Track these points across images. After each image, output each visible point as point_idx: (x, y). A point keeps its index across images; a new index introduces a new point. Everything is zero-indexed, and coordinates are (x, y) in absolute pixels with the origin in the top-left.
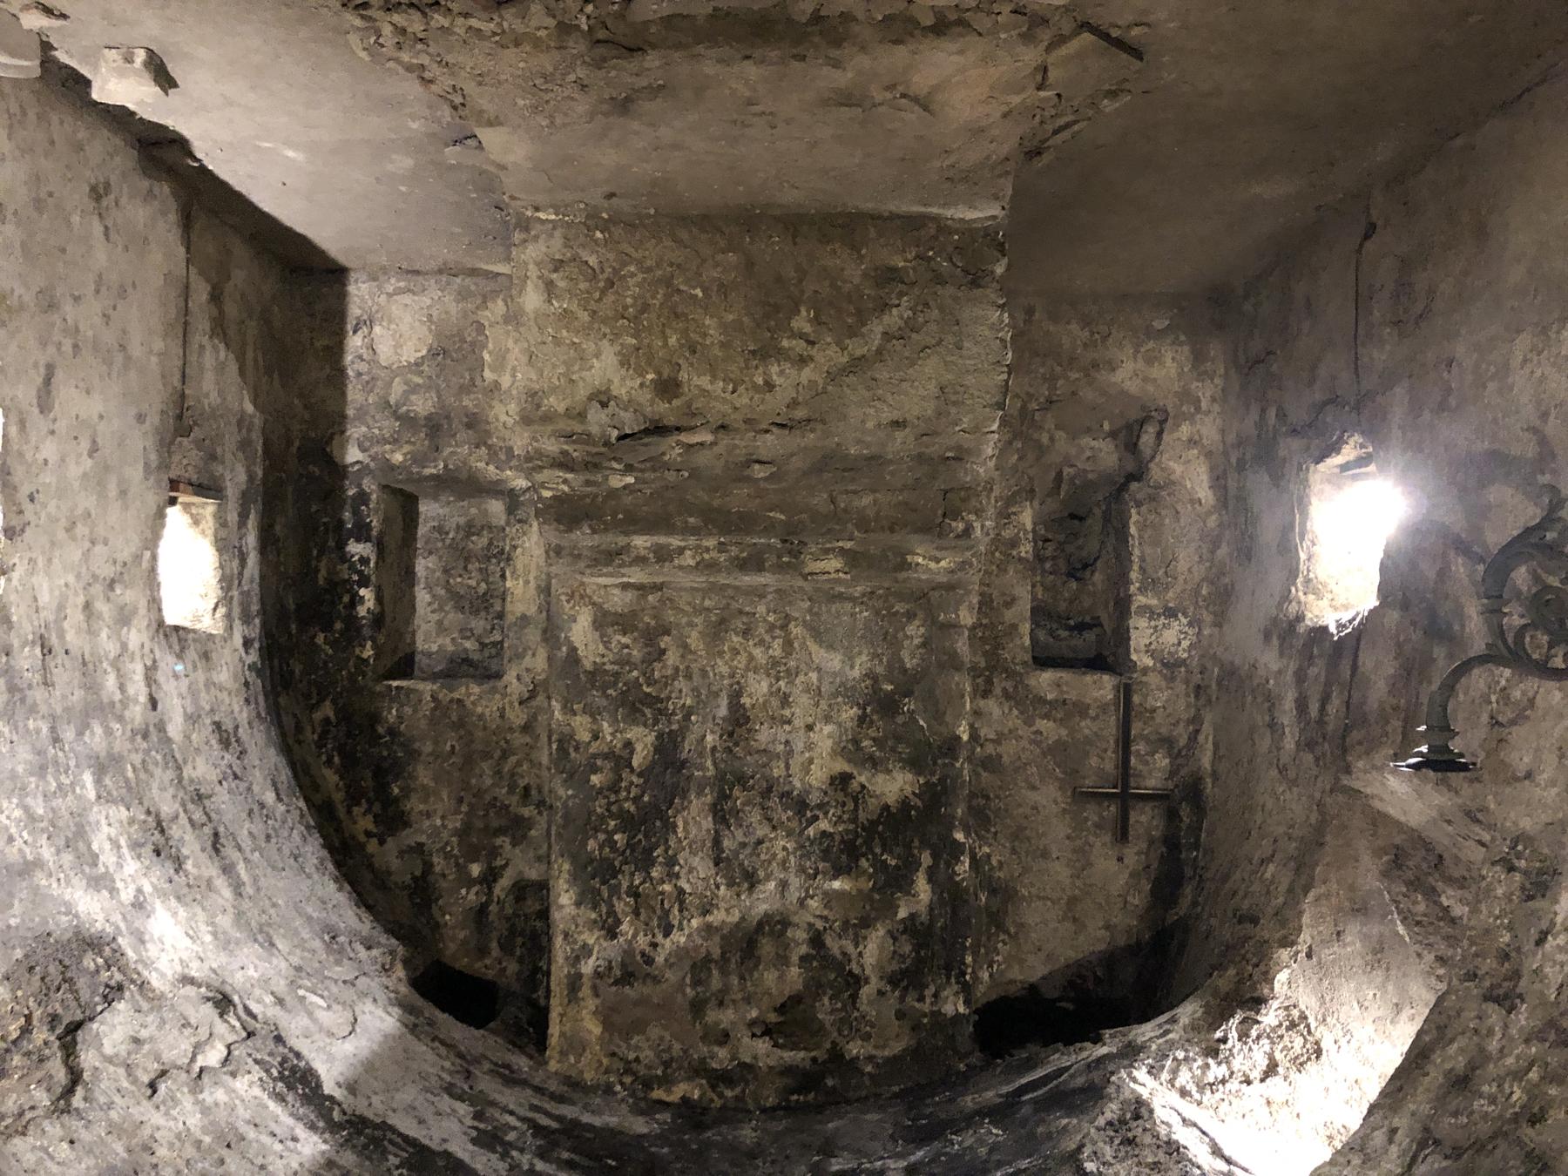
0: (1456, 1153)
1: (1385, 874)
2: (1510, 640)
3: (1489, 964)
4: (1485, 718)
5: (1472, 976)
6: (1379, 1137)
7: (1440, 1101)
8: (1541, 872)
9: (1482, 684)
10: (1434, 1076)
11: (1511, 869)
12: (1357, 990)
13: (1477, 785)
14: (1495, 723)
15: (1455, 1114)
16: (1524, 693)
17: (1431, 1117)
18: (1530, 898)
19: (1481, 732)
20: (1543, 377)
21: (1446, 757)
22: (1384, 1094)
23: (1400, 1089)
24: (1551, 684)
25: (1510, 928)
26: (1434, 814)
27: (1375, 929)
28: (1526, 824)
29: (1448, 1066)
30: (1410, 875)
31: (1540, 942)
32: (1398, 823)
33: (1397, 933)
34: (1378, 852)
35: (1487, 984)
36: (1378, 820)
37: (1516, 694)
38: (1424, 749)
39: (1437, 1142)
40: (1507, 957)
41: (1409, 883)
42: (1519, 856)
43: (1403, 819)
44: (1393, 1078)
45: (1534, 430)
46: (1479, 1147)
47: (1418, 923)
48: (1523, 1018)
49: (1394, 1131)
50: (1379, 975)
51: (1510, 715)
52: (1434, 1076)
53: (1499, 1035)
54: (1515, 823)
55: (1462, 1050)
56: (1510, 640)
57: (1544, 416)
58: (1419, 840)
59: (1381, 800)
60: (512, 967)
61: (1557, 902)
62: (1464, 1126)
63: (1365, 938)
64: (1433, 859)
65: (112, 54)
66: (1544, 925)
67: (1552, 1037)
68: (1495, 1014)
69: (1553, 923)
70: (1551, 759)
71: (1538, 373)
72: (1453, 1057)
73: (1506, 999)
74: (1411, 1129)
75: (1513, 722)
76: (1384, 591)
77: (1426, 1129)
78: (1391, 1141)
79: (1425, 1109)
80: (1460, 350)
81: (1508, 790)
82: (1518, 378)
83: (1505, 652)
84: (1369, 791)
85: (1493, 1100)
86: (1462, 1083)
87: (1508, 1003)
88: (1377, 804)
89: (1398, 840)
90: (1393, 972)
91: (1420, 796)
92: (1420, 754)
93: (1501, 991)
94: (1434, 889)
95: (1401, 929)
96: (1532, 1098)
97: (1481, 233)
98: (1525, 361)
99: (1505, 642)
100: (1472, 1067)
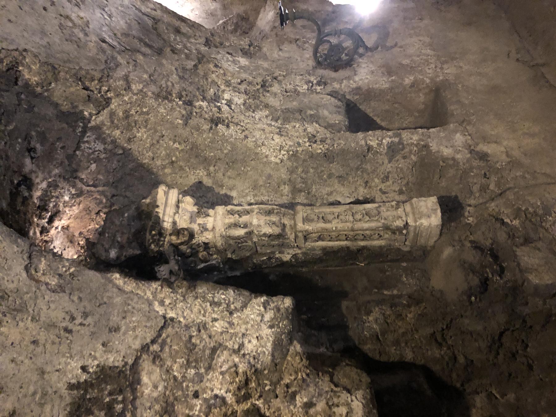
0: (156, 29)
1: (238, 15)
2: (325, 39)
3: (218, 40)
4: (298, 37)
5: (212, 35)
6: (152, 6)
7: (169, 24)
8: (251, 54)
9: (308, 36)
10: (178, 23)
11: (250, 46)
12: (197, 8)
13: (275, 36)
14: (297, 40)
15: (167, 28)
16: (307, 47)
17: (163, 22)
18: (241, 51)
19: (292, 36)
20: (414, 46)
21: (285, 20)
22: (166, 8)
23: (170, 13)
24: (311, 54)
25: (231, 45)
26: (262, 28)
27: (219, 13)
28: (265, 49)
29: (181, 27)
30: (240, 23)
31: (228, 53)
32: (257, 18)
33: (219, 21)
34: (245, 12)
35: (211, 39)
36: (257, 12)
37: (307, 45)
38: (287, 11)
39: (156, 23)
40: (221, 44)
41: (237, 23)
42: (254, 48)
43: (259, 19)
44: (173, 12)
45: (396, 45)
46: (159, 35)
47: (224, 28)
48: (203, 49)
49: (155, 10)
50: (204, 15)
51: (300, 44)
52: (178, 23)
53: (196, 42)
54: (264, 47)
55: (188, 31)
56: (325, 39)
57: (401, 47)
58: (252, 26)
59: (264, 11)
60: (128, 389)
61: (242, 57)
62: (164, 32)
63: (215, 10)
64: (247, 31)
65: (166, 384)
66: (234, 54)
67: (200, 56)
68: (203, 40)
69: (235, 57)
70: (287, 55)
71: (415, 44)
72: (185, 29)
73: (207, 43)
74: (158, 15)
75: (297, 45)
76: (338, 6)
77: (159, 20)
78: (151, 9)
79: (166, 21)
80: (426, 22)
81: (275, 44)
82: (415, 39)
83: (322, 36)
84: (267, 7)
85: (175, 40)
86: (178, 31)
87: (206, 44)
88: (262, 10)
89: (251, 19)
90: (206, 20)
91: (267, 23)
92: (285, 11)
93: (210, 43)
94: (236, 32)
95: (221, 22)
96: (180, 50)
97: (469, 24)
98: (420, 40)
99: (325, 37)
100: (184, 34)
